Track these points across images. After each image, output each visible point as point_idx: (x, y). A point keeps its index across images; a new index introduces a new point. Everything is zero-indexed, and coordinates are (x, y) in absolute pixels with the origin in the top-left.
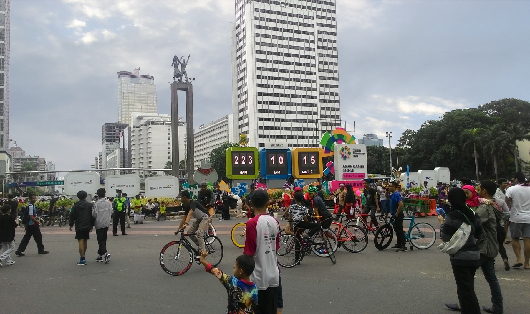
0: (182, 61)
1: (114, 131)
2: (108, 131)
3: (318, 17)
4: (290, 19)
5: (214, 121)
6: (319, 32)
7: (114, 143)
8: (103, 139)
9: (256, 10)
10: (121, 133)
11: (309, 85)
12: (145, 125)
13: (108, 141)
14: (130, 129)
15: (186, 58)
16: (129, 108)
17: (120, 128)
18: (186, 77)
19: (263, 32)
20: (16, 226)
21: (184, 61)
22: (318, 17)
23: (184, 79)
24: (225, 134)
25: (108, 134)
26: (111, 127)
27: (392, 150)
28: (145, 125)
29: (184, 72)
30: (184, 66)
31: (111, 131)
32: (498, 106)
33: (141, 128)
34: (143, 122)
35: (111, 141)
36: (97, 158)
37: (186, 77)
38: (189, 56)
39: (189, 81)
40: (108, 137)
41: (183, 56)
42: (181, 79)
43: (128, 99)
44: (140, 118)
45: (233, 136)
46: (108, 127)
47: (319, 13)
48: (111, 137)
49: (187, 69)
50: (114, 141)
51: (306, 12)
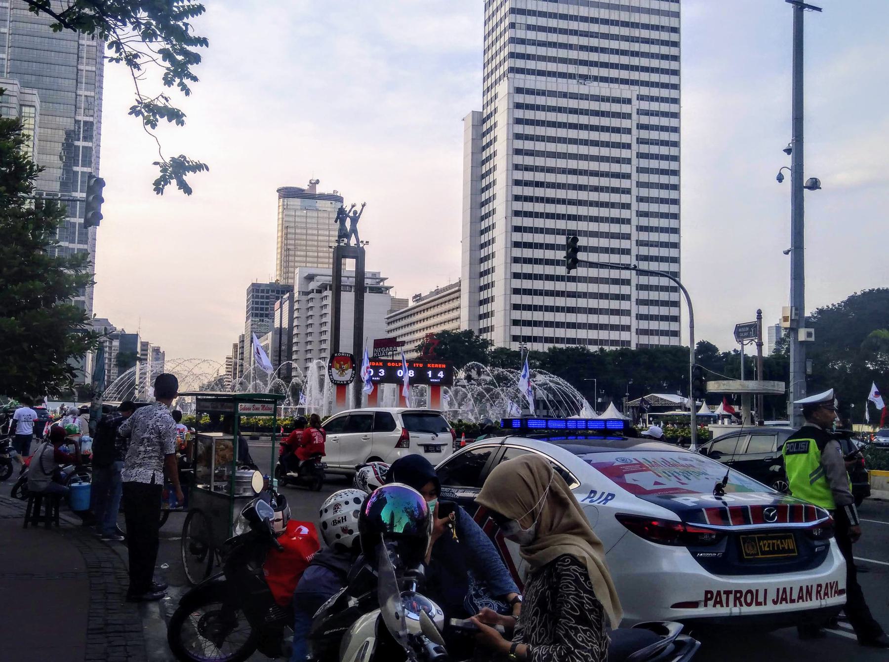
0: (351, 214)
1: (268, 297)
2: (257, 297)
3: (641, 98)
4: (584, 105)
5: (441, 286)
6: (641, 127)
7: (266, 319)
8: (247, 312)
9: (519, 90)
10: (278, 303)
11: (615, 228)
12: (319, 291)
13: (256, 315)
14: (291, 298)
15: (358, 208)
16: (295, 256)
17: (278, 292)
18: (357, 239)
19: (529, 130)
20: (685, 530)
21: (355, 212)
22: (641, 98)
23: (353, 242)
24: (454, 314)
25: (257, 303)
26: (263, 291)
27: (746, 356)
28: (319, 291)
29: (354, 230)
30: (355, 220)
31: (262, 297)
32: (852, 302)
33: (310, 296)
34: (313, 285)
35: (262, 315)
36: (235, 346)
37: (357, 239)
38: (363, 206)
39: (361, 245)
40: (257, 309)
41: (353, 206)
42: (349, 241)
43: (295, 240)
44: (310, 278)
45: (467, 318)
46: (257, 291)
47: (645, 91)
48: (262, 309)
49: (359, 226)
50: (267, 316)
51: (617, 90)
